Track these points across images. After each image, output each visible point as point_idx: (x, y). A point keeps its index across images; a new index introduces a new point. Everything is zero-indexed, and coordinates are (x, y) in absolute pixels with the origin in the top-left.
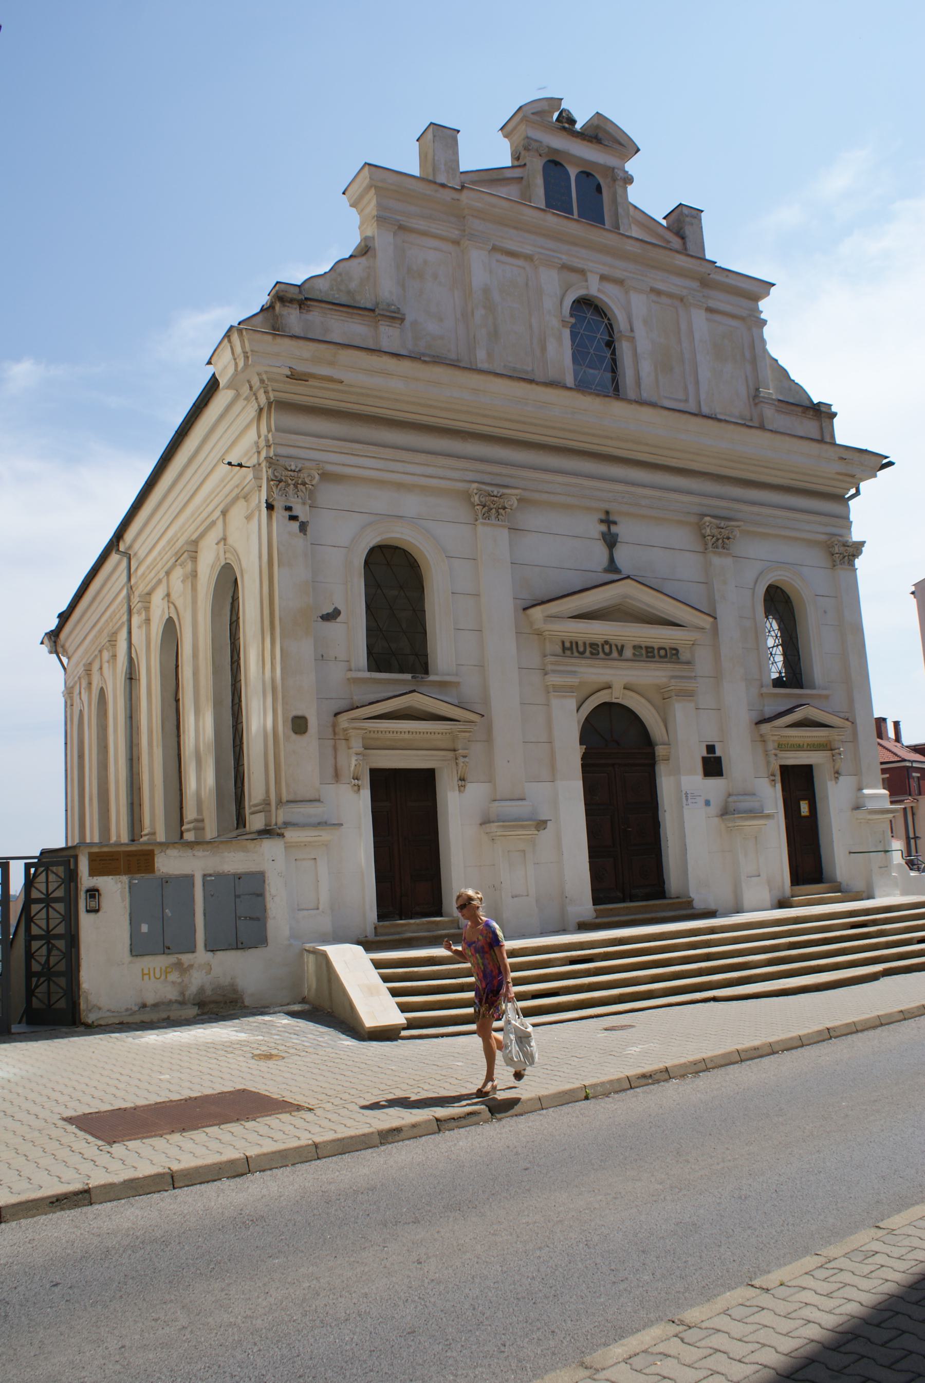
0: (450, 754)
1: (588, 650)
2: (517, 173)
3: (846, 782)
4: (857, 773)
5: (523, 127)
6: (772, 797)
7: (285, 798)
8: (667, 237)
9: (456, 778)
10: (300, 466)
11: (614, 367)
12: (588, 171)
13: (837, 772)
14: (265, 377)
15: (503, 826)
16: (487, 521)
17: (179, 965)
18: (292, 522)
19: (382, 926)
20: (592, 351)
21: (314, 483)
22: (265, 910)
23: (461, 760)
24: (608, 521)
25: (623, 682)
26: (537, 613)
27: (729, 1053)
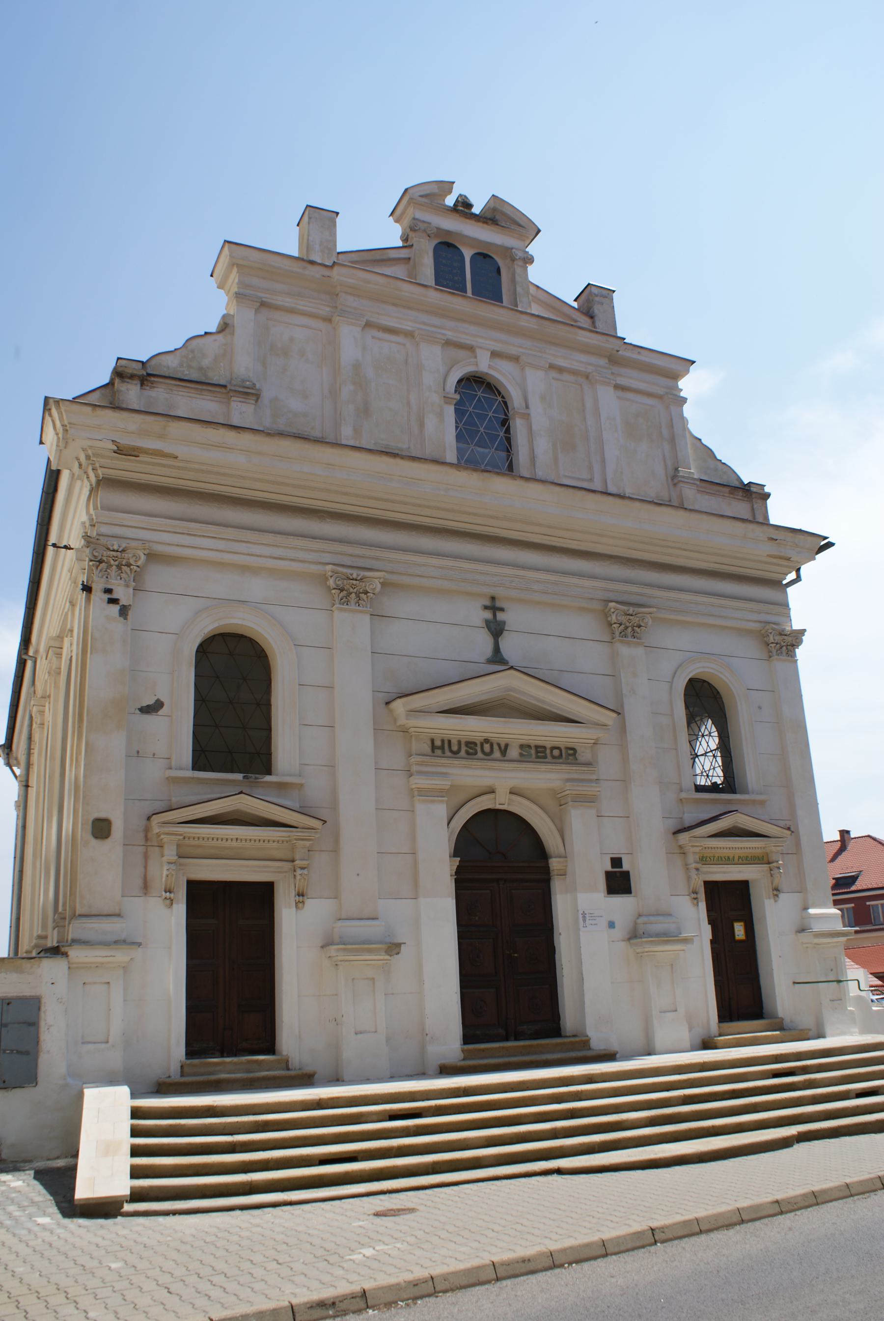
0: (287, 866)
1: (464, 748)
2: (404, 253)
4: (802, 890)
5: (410, 210)
8: (574, 316)
9: (293, 894)
10: (124, 545)
11: (508, 445)
12: (485, 252)
14: (90, 452)
15: (344, 949)
16: (345, 607)
18: (111, 605)
19: (189, 1065)
20: (482, 429)
21: (139, 564)
22: (38, 1042)
23: (299, 872)
24: (493, 607)
25: (505, 785)
26: (399, 706)
27: (478, 1268)
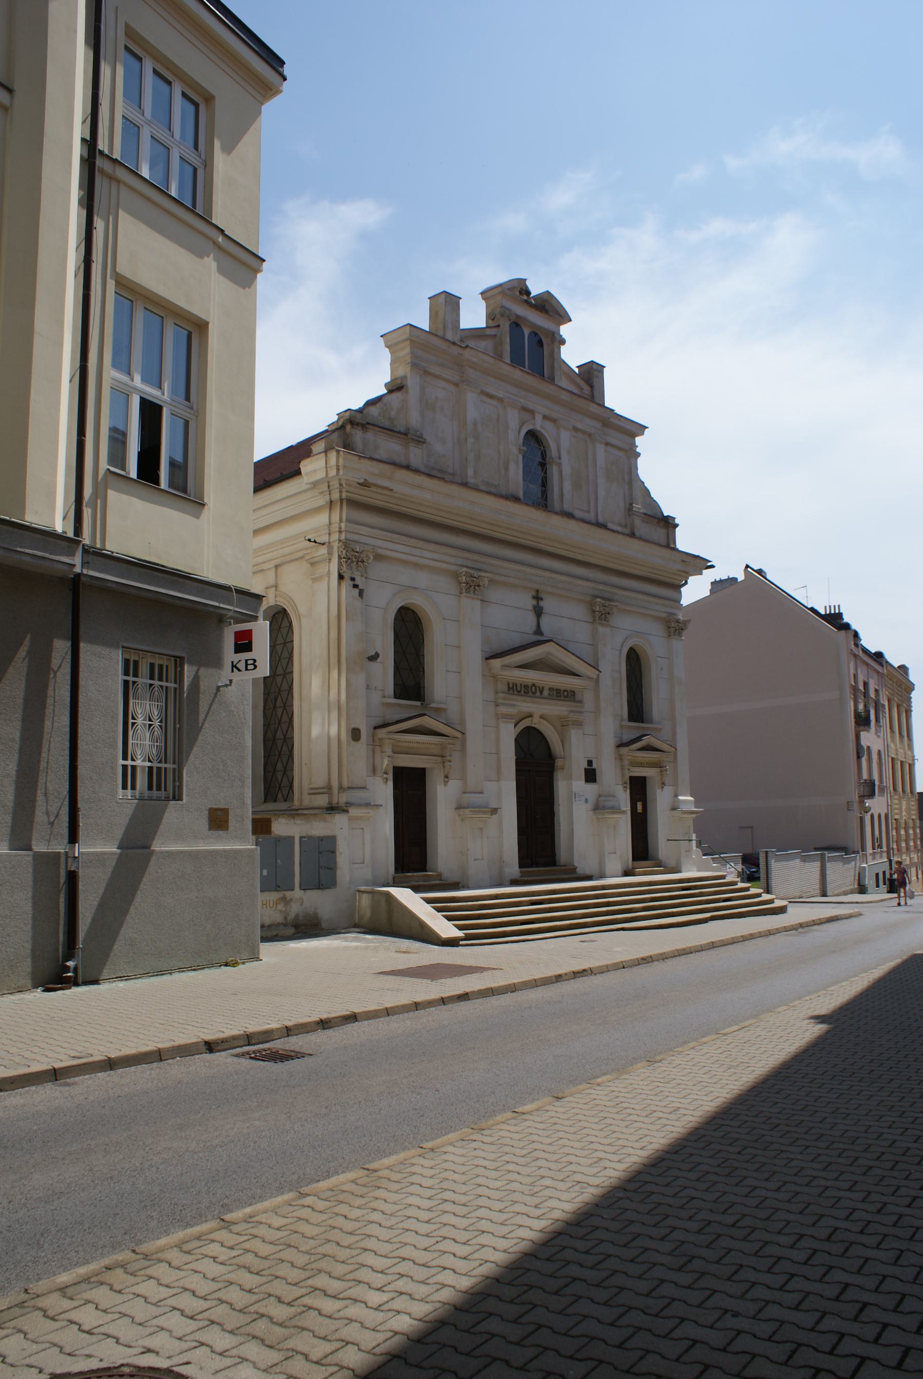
0: (439, 759)
3: (668, 790)
4: (675, 785)
6: (623, 798)
7: (345, 784)
13: (663, 783)
14: (343, 482)
17: (285, 900)
23: (448, 764)
24: (537, 598)
25: (541, 712)
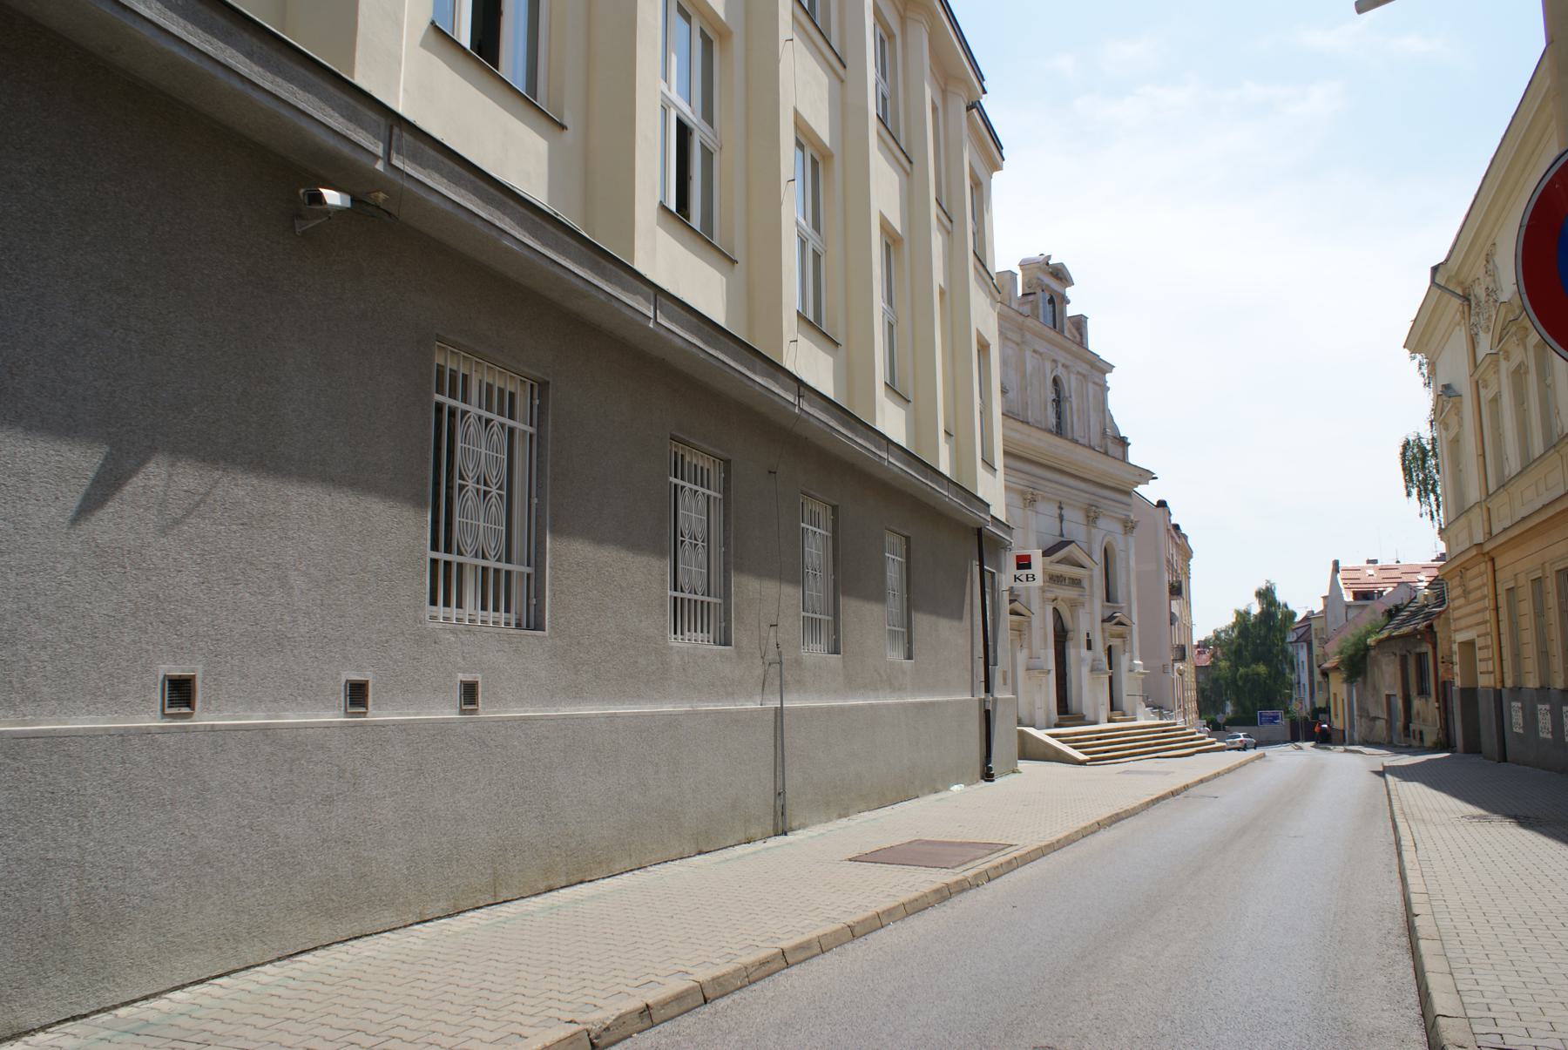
24: (1061, 508)
25: (1116, 642)
